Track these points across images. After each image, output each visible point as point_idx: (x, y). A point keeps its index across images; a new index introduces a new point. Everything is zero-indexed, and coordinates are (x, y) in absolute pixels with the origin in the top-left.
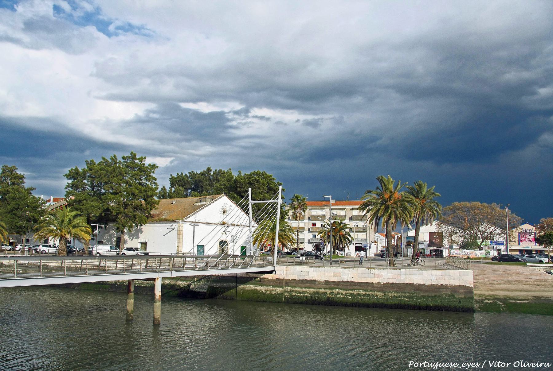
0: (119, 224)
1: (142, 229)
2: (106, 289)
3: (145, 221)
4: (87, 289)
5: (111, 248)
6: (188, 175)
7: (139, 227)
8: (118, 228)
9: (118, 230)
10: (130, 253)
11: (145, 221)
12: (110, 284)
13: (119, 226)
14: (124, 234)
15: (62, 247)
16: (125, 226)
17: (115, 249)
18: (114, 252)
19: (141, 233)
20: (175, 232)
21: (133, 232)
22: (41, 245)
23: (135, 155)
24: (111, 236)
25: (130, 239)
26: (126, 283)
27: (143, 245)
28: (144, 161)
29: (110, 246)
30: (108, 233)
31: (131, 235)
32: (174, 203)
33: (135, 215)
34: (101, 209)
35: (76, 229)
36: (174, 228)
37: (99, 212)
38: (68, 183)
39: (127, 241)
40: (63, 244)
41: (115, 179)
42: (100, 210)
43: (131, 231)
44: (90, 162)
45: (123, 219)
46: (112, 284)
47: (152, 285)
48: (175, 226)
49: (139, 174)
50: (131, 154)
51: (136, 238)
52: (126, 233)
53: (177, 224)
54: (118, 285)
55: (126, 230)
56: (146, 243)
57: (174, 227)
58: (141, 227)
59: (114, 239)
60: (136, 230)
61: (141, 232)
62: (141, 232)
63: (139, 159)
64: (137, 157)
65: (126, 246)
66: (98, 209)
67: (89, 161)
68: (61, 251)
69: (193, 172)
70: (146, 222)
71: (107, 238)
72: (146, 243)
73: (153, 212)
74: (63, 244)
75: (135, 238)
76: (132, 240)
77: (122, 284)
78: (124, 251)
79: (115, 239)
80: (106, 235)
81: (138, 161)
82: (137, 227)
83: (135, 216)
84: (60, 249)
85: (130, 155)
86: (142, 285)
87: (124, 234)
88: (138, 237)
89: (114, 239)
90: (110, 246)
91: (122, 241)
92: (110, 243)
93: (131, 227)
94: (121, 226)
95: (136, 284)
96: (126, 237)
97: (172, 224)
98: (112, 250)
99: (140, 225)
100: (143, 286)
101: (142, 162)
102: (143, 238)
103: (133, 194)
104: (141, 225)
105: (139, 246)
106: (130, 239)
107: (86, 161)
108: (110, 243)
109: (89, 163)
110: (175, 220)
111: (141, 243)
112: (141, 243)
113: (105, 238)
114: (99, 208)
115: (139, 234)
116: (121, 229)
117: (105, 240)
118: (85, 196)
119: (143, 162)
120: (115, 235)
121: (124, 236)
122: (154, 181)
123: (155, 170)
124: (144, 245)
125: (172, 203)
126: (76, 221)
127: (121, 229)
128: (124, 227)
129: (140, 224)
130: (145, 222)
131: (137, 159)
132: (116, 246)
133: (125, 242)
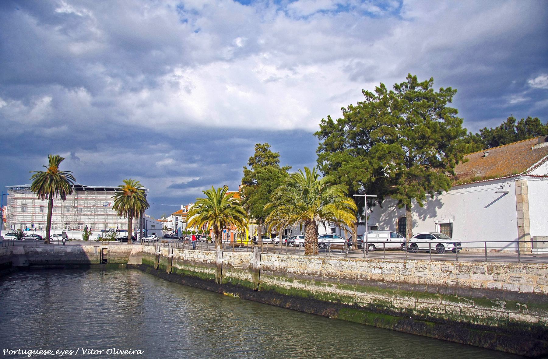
0: (401, 194)
1: (440, 199)
2: (389, 324)
3: (448, 185)
4: (351, 320)
5: (392, 236)
6: (479, 133)
7: (435, 197)
8: (400, 201)
9: (400, 205)
10: (422, 244)
11: (448, 185)
12: (397, 313)
13: (401, 198)
14: (410, 211)
15: (310, 238)
16: (413, 197)
17: (398, 237)
18: (397, 242)
19: (440, 208)
20: (511, 198)
21: (425, 207)
22: (298, 236)
23: (415, 79)
24: (391, 216)
25: (420, 218)
26: (433, 313)
27: (446, 228)
28: (431, 86)
29: (389, 232)
30: (385, 211)
31: (422, 211)
32: (487, 154)
33: (429, 176)
34: (369, 170)
35: (329, 206)
36: (506, 191)
37: (367, 174)
38: (320, 144)
39: (415, 223)
40: (311, 232)
41: (388, 117)
42: (367, 171)
43: (421, 205)
44: (347, 109)
45: (408, 184)
46: (401, 314)
47: (503, 324)
48: (510, 186)
49: (426, 105)
50: (407, 78)
51: (430, 217)
52: (414, 209)
53: (513, 183)
54: (414, 316)
55: (414, 203)
56: (450, 225)
57: (506, 189)
58: (439, 197)
59: (394, 220)
60: (430, 203)
61: (440, 205)
62: (440, 205)
63: (422, 85)
64: (419, 81)
65: (416, 231)
66: (365, 169)
67: (346, 107)
68: (309, 245)
69: (485, 129)
70: (448, 187)
71: (385, 220)
72: (450, 225)
73: (458, 170)
74: (311, 232)
75: (428, 216)
76: (424, 220)
77: (425, 316)
78: (414, 240)
79: (397, 219)
80: (383, 215)
81: (420, 88)
82: (432, 197)
83: (428, 178)
84: (308, 242)
85: (407, 81)
86: (474, 321)
87: (410, 211)
88: (434, 215)
89: (394, 220)
90: (389, 232)
91: (408, 222)
92: (389, 226)
93: (422, 197)
94: (405, 197)
95: (458, 317)
96: (415, 216)
97: (501, 184)
98: (393, 240)
99: (438, 193)
100: (476, 323)
101: (427, 89)
102: (442, 216)
103: (423, 137)
104: (440, 193)
105: (437, 230)
106: (420, 218)
107: (341, 109)
108: (389, 226)
109: (347, 111)
110: (509, 175)
111: (441, 225)
112: (441, 225)
113: (382, 219)
114: (366, 168)
115: (437, 209)
116: (405, 202)
117: (382, 222)
118: (344, 156)
119: (429, 88)
120: (397, 214)
121: (411, 214)
122: (453, 115)
123: (451, 96)
124: (447, 227)
125: (484, 156)
126: (330, 191)
127: (406, 202)
128: (410, 198)
129: (438, 191)
130: (446, 187)
131: (418, 85)
132: (398, 231)
133: (414, 224)
